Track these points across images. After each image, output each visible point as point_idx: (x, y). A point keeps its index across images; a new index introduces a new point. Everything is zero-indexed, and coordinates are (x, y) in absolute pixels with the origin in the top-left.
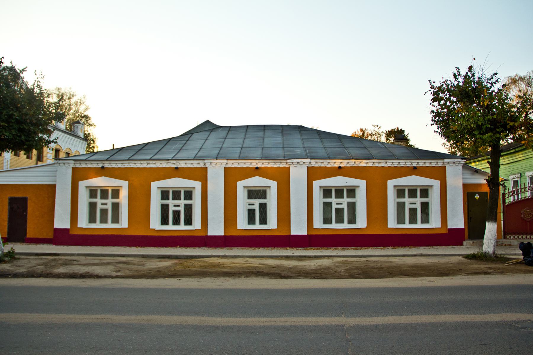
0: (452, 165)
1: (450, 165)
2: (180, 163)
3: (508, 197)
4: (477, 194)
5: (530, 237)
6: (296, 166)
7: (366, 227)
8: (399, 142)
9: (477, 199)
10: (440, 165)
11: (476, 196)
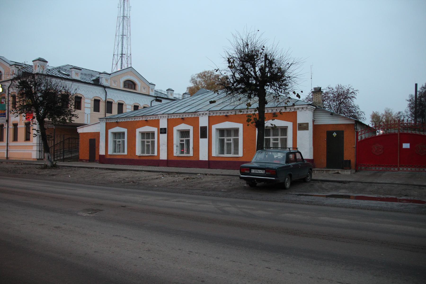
0: (301, 110)
1: (300, 110)
2: (148, 118)
3: (361, 135)
4: (335, 133)
5: (424, 170)
6: (305, 110)
7: (242, 156)
8: (315, 93)
9: (335, 136)
10: (288, 111)
11: (334, 134)
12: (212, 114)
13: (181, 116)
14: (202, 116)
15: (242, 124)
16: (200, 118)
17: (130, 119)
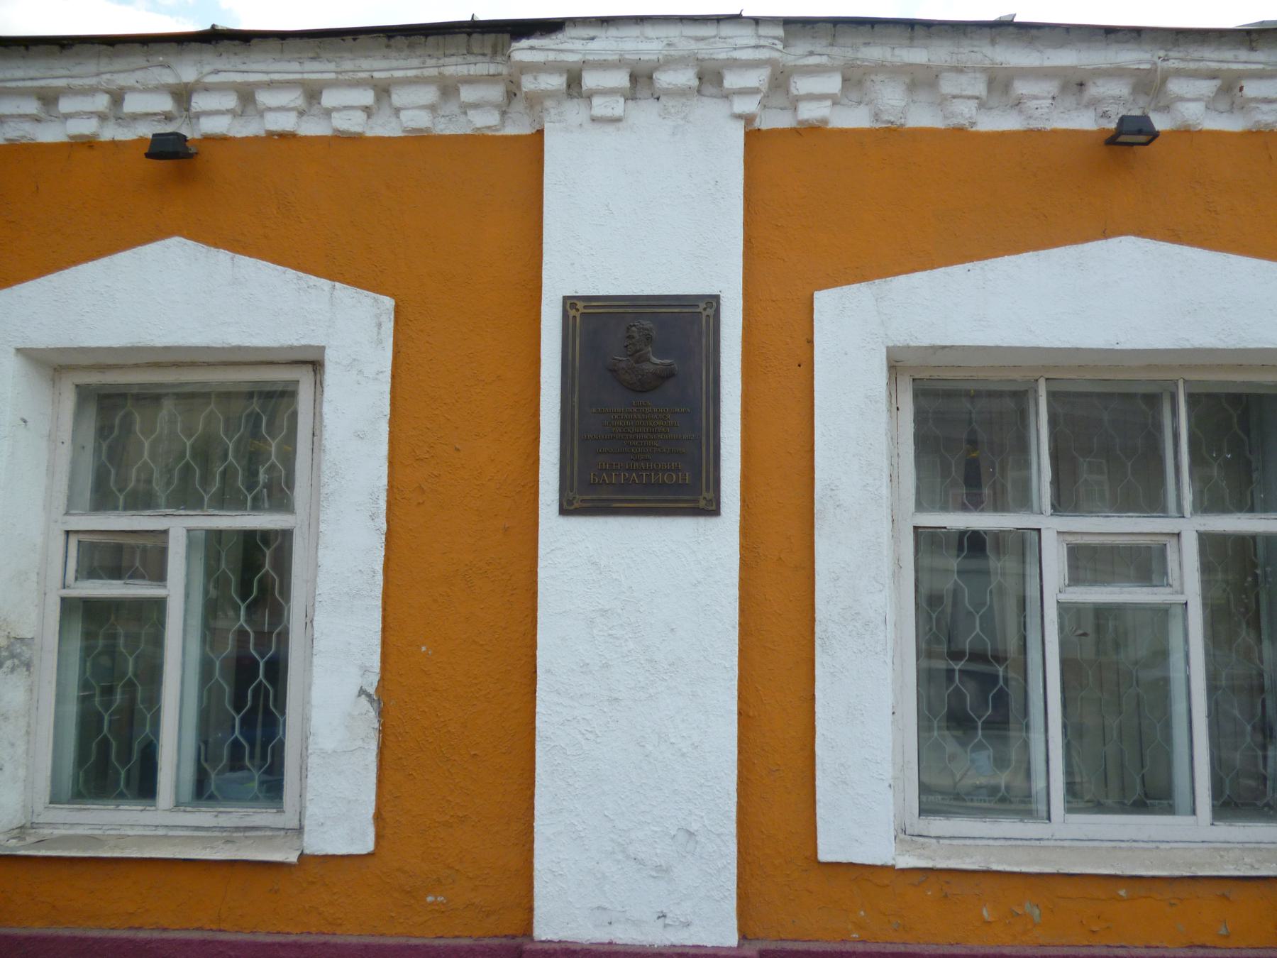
12: (833, 84)
13: (132, 104)
14: (616, 107)
15: (826, 302)
16: (551, 143)
17: (468, 94)
